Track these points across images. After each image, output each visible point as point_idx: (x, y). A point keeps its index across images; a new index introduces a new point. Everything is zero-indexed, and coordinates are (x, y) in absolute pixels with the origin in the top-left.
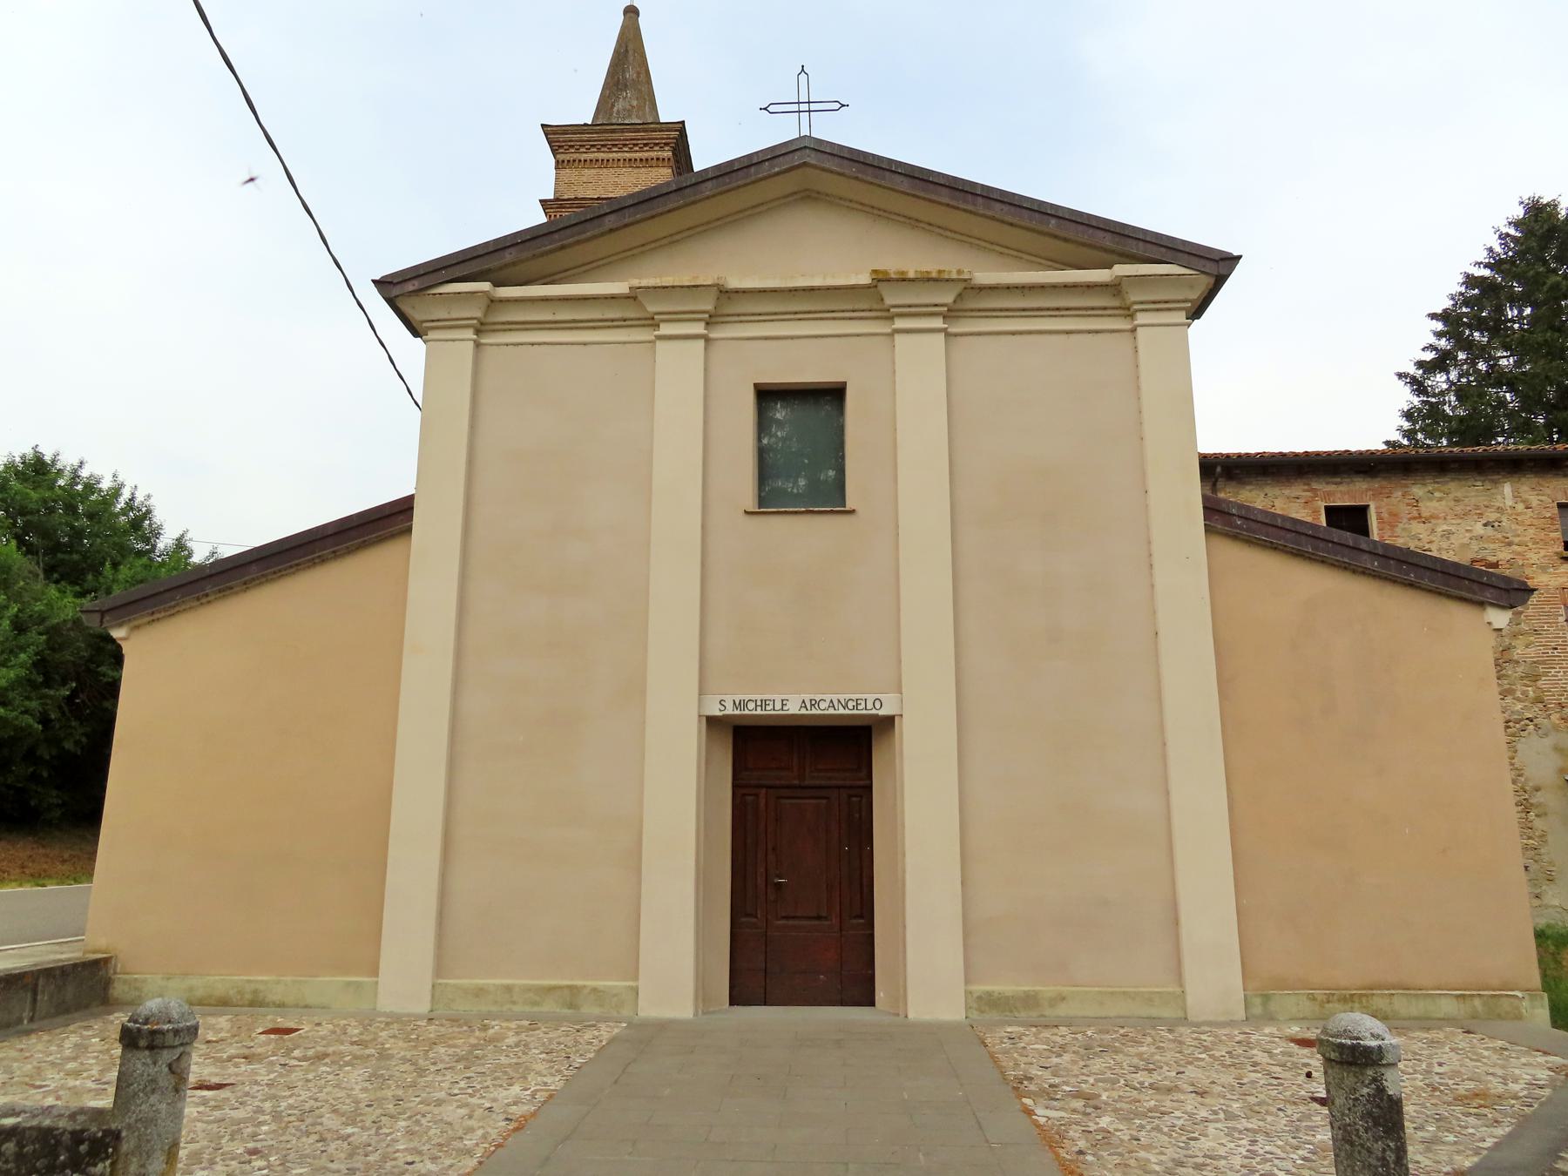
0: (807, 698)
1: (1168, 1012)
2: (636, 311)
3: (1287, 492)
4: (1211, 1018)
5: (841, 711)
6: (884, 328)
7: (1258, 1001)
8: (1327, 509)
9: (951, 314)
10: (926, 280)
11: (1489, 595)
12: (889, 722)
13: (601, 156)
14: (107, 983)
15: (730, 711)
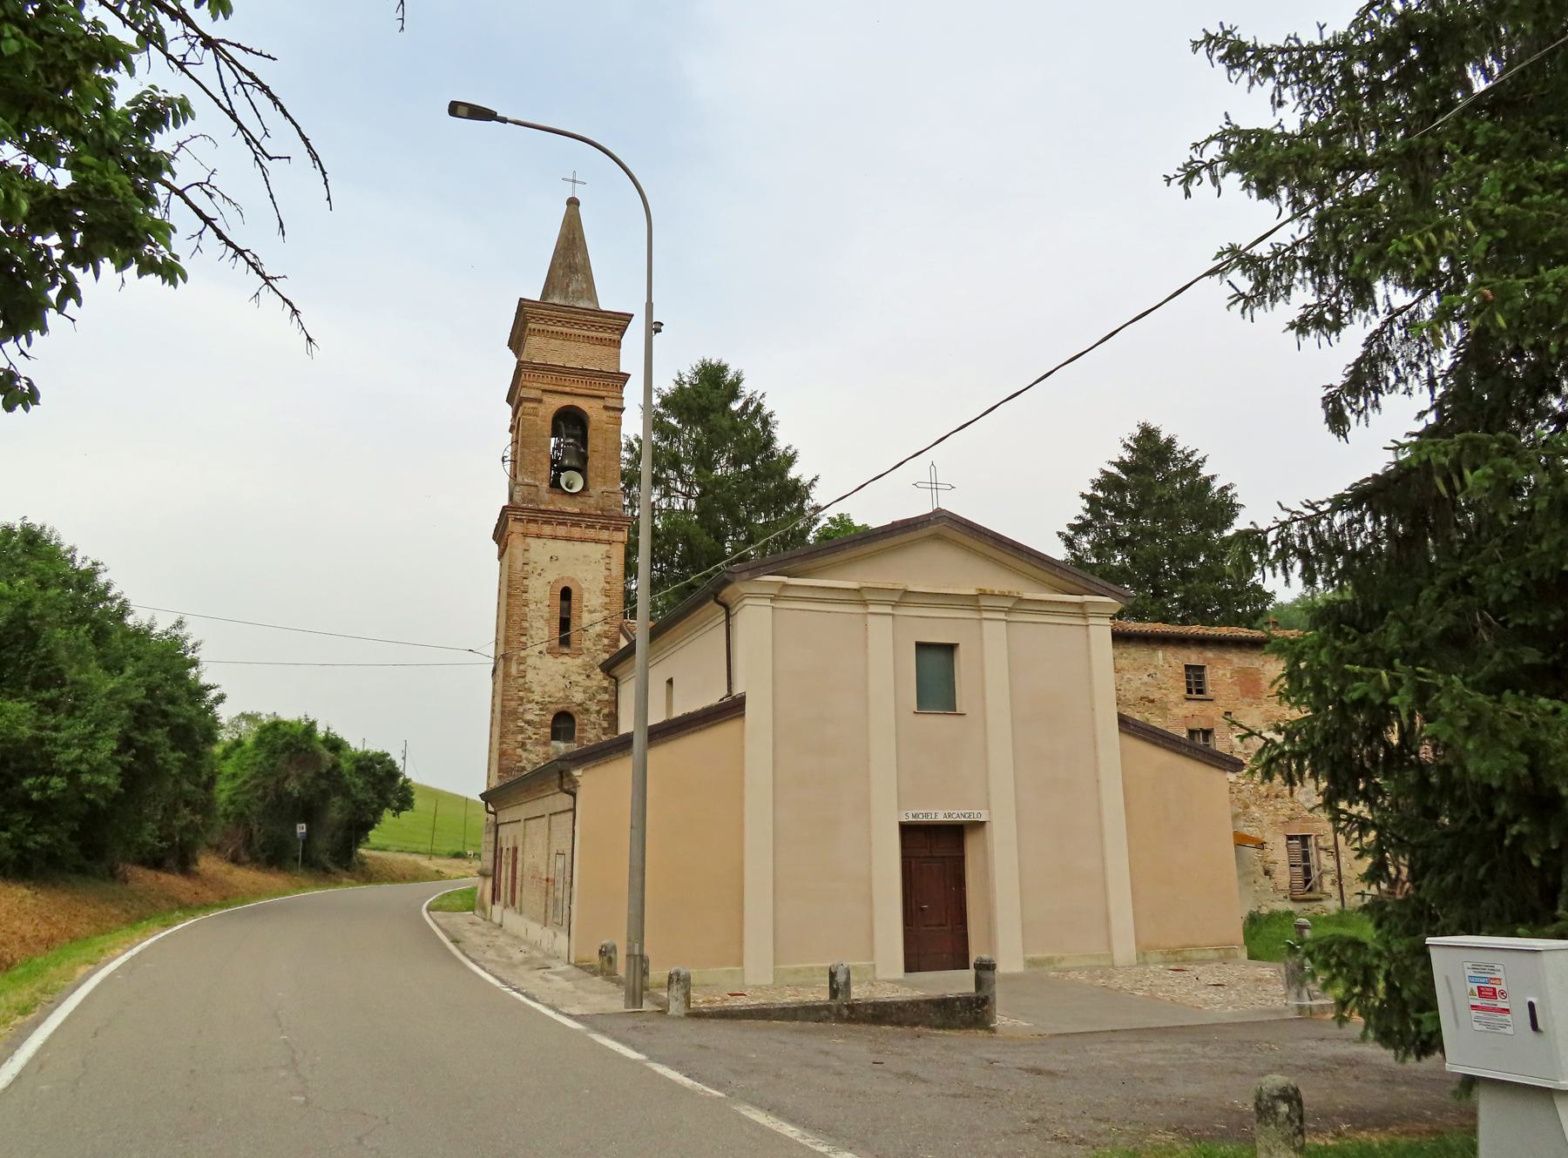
2: (859, 597)
9: (1010, 611)
10: (1003, 596)
12: (979, 825)
13: (565, 330)
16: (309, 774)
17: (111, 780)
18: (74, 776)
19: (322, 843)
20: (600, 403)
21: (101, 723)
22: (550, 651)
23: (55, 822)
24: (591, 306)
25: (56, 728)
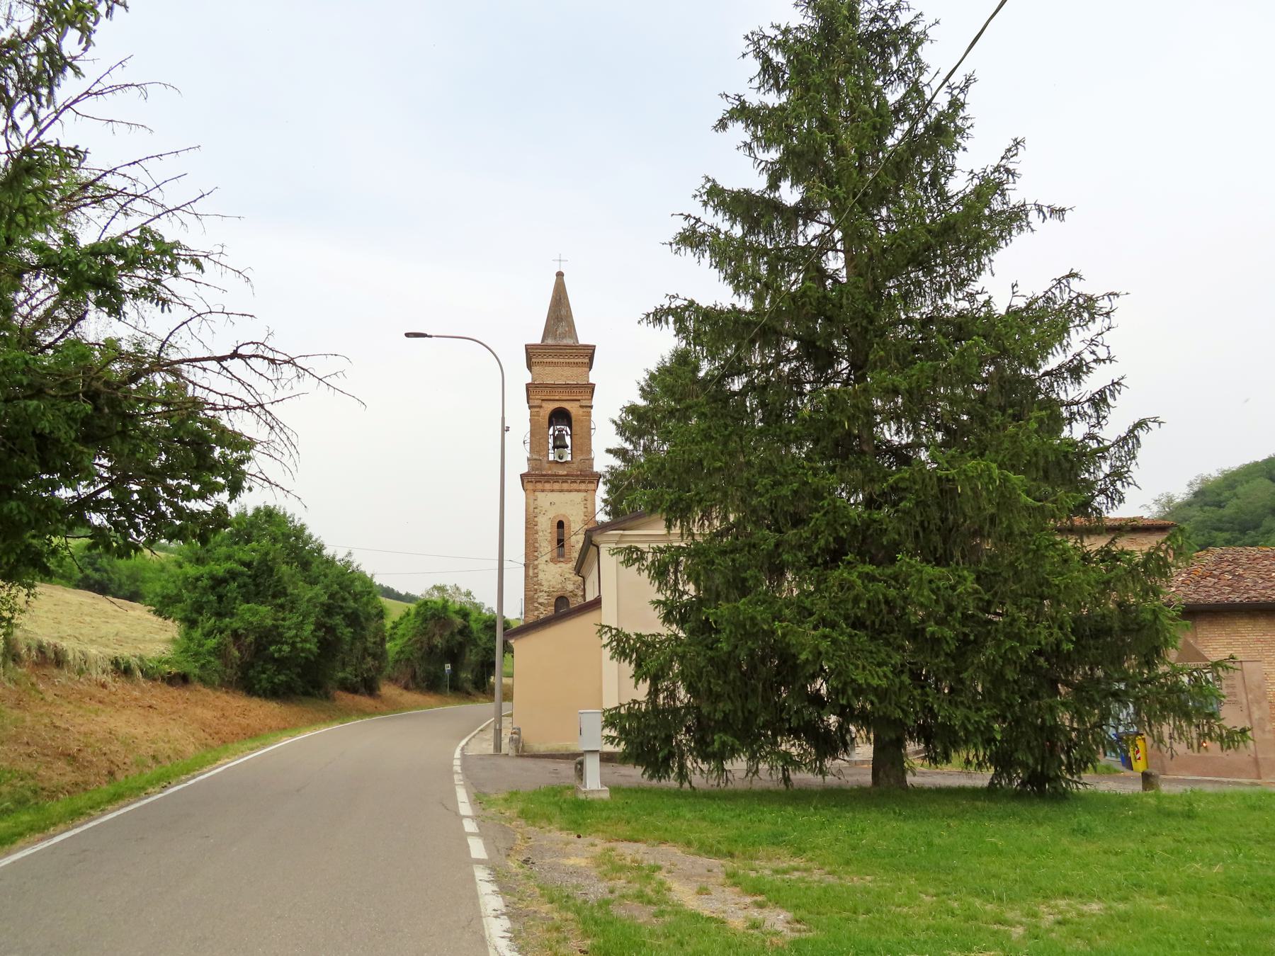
16: (447, 633)
17: (312, 646)
18: (293, 645)
19: (465, 675)
20: (578, 404)
21: (305, 616)
22: (552, 560)
23: (289, 669)
24: (569, 342)
25: (284, 619)
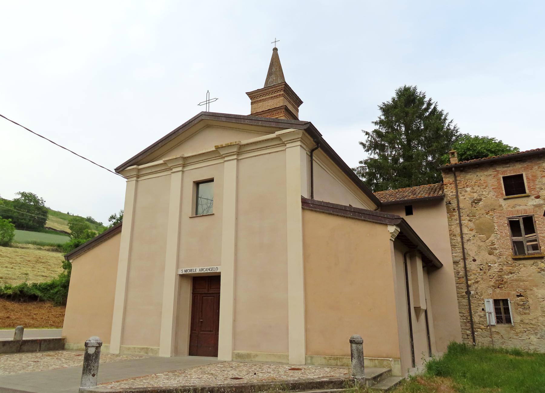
0: (201, 268)
1: (284, 361)
3: (486, 173)
4: (295, 363)
5: (209, 271)
6: (221, 161)
7: (309, 358)
8: (504, 178)
11: (387, 221)
14: (64, 345)
15: (184, 273)
